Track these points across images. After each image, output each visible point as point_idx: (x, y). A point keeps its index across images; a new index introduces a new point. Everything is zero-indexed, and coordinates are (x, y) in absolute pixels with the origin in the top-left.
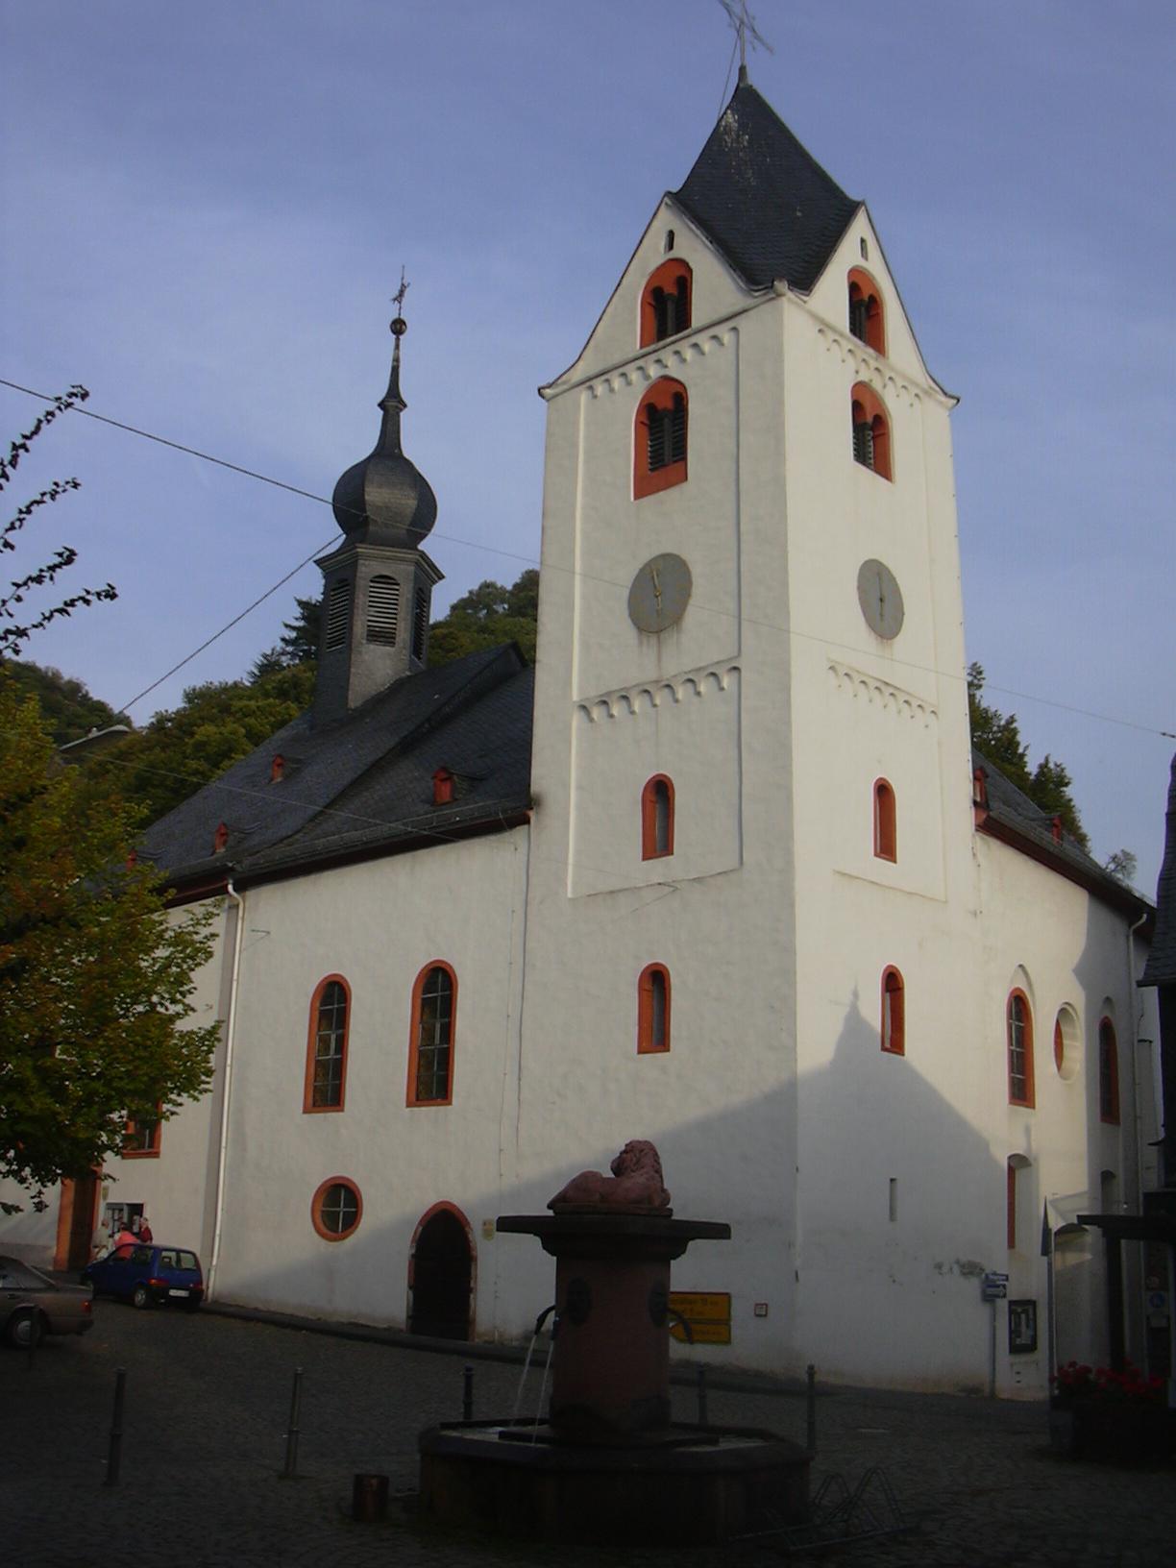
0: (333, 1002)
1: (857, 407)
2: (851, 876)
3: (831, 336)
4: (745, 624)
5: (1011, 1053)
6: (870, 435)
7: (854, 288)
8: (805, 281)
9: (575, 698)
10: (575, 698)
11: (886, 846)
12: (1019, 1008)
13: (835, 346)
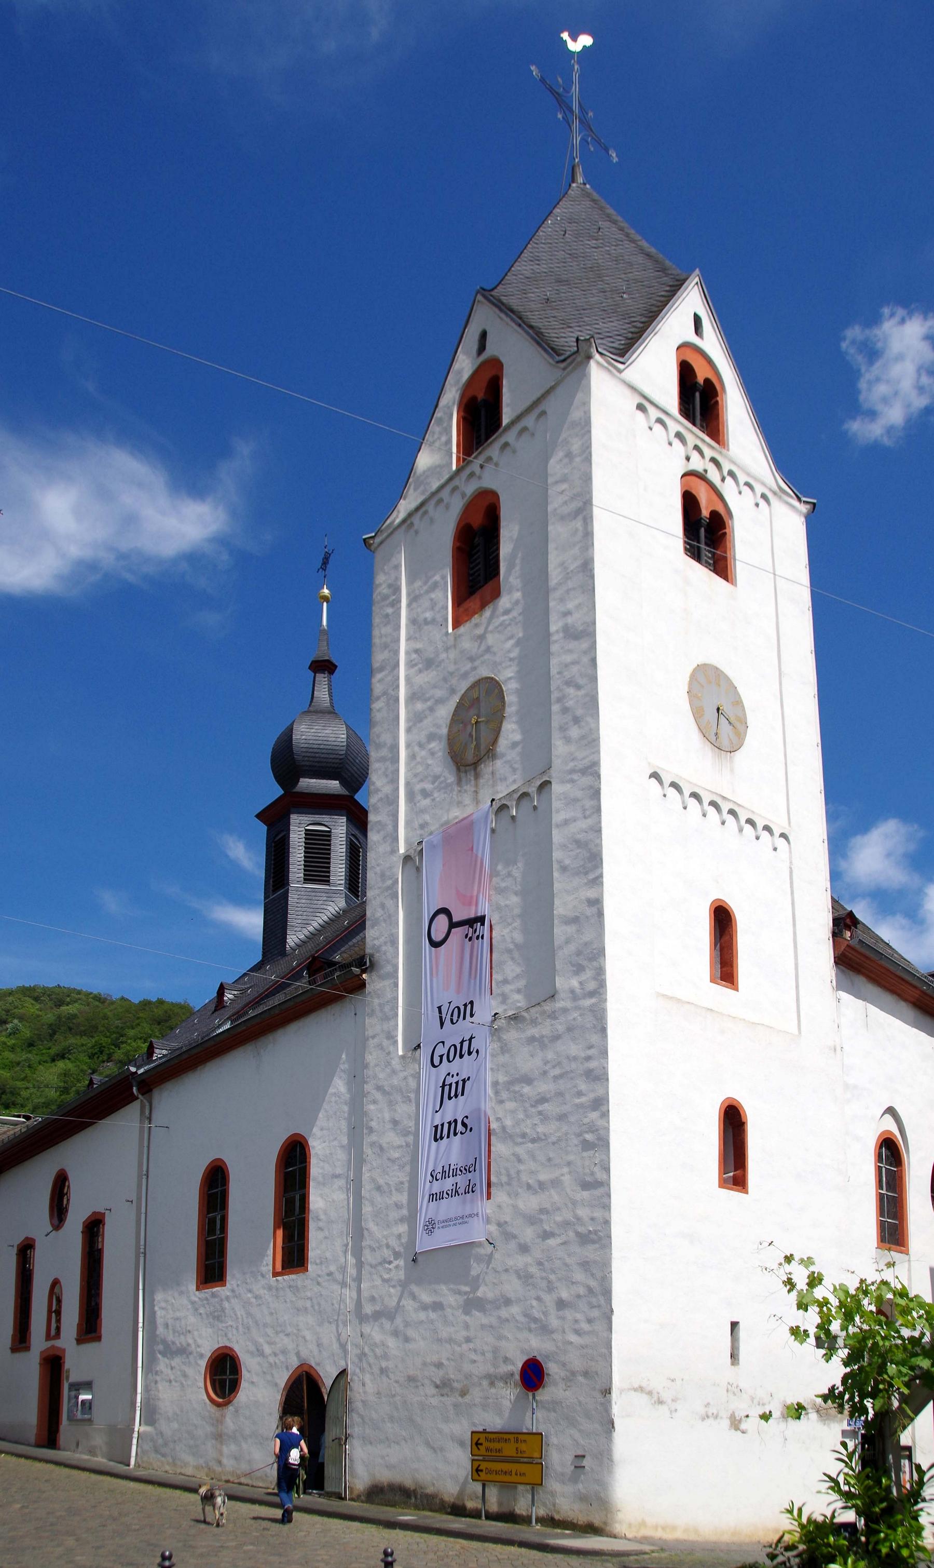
0: (216, 1181)
1: (690, 502)
2: (679, 1001)
3: (654, 413)
4: (481, 1495)
5: (881, 1197)
6: (706, 534)
7: (686, 372)
8: (625, 346)
9: (402, 850)
10: (402, 850)
11: (725, 969)
12: (890, 1152)
13: (658, 428)
